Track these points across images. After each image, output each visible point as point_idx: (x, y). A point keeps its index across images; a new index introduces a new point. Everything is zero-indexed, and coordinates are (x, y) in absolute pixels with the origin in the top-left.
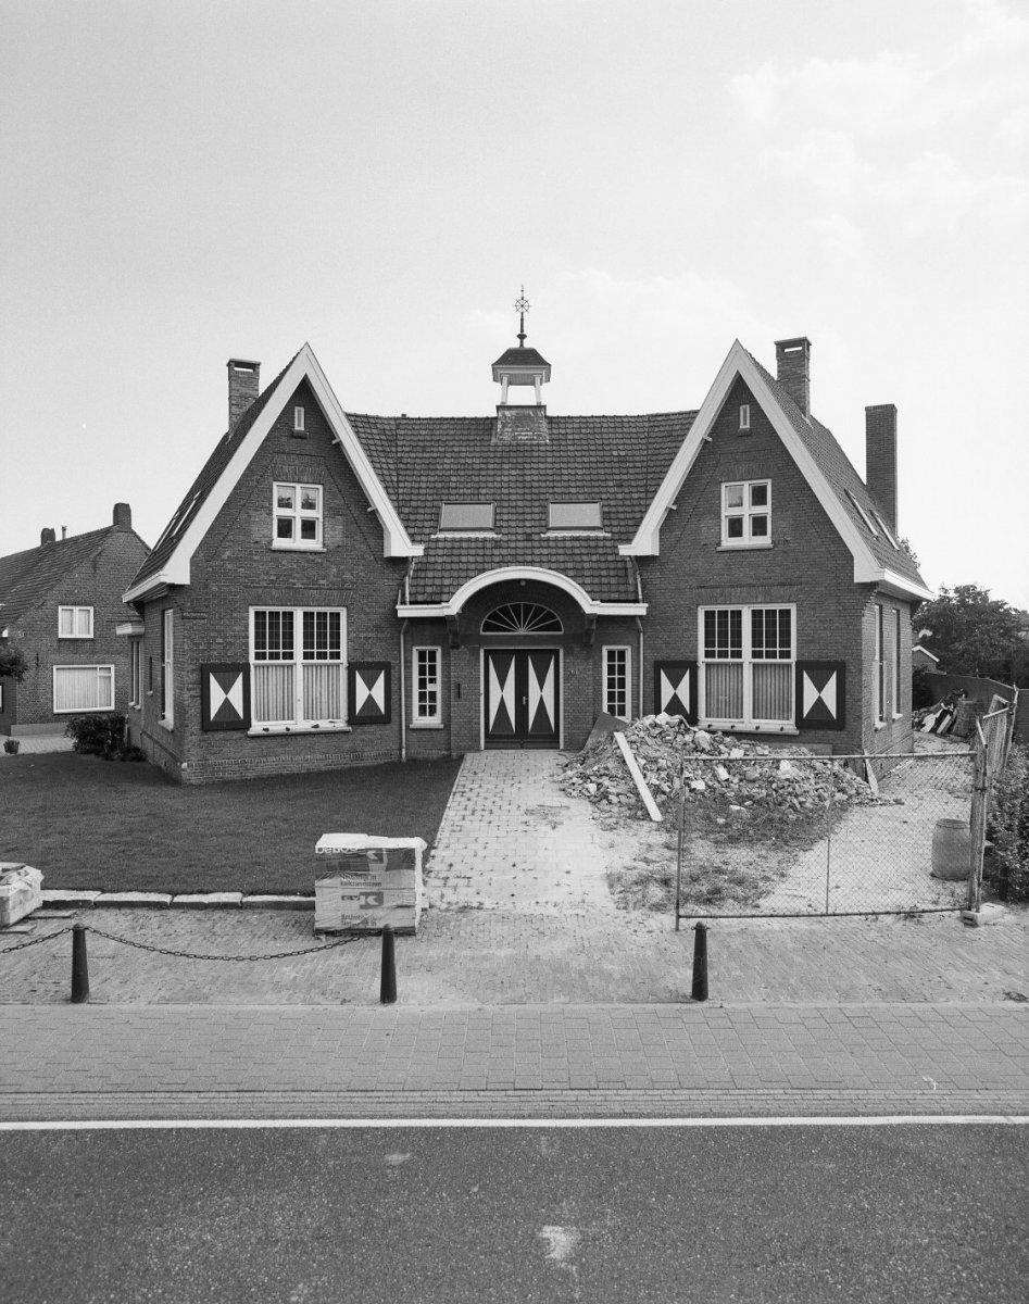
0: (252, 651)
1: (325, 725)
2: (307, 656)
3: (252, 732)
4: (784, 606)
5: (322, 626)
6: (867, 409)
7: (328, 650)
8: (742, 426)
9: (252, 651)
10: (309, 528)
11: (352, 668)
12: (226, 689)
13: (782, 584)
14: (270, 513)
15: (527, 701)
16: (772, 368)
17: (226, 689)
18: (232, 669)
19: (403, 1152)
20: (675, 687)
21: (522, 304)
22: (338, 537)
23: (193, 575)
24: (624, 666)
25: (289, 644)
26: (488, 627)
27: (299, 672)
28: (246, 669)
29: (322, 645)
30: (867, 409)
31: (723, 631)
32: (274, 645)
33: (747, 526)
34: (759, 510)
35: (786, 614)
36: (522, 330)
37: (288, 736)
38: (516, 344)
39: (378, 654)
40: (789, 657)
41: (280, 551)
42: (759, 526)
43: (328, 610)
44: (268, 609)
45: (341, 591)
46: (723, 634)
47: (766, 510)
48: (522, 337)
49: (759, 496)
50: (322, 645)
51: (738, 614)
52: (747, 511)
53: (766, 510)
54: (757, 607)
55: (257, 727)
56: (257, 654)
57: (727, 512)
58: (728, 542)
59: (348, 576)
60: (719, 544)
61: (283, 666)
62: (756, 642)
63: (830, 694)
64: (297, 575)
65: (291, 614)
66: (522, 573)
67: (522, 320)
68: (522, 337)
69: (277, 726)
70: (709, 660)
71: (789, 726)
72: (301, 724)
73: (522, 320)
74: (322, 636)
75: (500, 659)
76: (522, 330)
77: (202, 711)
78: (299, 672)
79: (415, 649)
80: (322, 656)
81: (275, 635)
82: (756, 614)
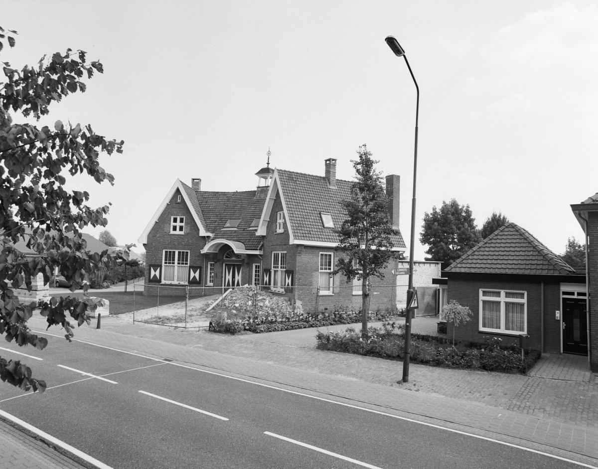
0: (163, 261)
1: (182, 283)
2: (179, 263)
3: (162, 283)
4: (187, 251)
5: (183, 255)
7: (171, 262)
8: (178, 201)
9: (163, 261)
10: (181, 229)
11: (190, 267)
12: (155, 271)
13: (285, 245)
14: (170, 224)
16: (190, 185)
17: (155, 271)
18: (157, 266)
20: (195, 276)
21: (269, 153)
22: (188, 231)
23: (148, 241)
25: (174, 260)
26: (227, 257)
27: (176, 268)
28: (161, 266)
29: (183, 261)
31: (170, 257)
32: (183, 261)
33: (178, 228)
34: (175, 224)
35: (187, 253)
37: (171, 285)
38: (265, 166)
39: (198, 264)
41: (173, 235)
42: (181, 229)
43: (185, 251)
44: (168, 250)
45: (188, 246)
46: (183, 258)
47: (183, 224)
48: (268, 164)
49: (182, 221)
50: (170, 260)
51: (174, 252)
52: (178, 224)
53: (183, 224)
54: (166, 250)
55: (163, 282)
56: (321, 268)
57: (279, 221)
58: (172, 232)
59: (190, 241)
60: (170, 232)
61: (185, 267)
62: (179, 260)
63: (197, 275)
64: (176, 242)
65: (175, 252)
68: (268, 164)
69: (168, 282)
70: (275, 269)
71: (187, 283)
72: (175, 282)
74: (183, 258)
75: (229, 266)
78: (176, 268)
79: (254, 264)
80: (170, 263)
81: (170, 257)
82: (179, 252)
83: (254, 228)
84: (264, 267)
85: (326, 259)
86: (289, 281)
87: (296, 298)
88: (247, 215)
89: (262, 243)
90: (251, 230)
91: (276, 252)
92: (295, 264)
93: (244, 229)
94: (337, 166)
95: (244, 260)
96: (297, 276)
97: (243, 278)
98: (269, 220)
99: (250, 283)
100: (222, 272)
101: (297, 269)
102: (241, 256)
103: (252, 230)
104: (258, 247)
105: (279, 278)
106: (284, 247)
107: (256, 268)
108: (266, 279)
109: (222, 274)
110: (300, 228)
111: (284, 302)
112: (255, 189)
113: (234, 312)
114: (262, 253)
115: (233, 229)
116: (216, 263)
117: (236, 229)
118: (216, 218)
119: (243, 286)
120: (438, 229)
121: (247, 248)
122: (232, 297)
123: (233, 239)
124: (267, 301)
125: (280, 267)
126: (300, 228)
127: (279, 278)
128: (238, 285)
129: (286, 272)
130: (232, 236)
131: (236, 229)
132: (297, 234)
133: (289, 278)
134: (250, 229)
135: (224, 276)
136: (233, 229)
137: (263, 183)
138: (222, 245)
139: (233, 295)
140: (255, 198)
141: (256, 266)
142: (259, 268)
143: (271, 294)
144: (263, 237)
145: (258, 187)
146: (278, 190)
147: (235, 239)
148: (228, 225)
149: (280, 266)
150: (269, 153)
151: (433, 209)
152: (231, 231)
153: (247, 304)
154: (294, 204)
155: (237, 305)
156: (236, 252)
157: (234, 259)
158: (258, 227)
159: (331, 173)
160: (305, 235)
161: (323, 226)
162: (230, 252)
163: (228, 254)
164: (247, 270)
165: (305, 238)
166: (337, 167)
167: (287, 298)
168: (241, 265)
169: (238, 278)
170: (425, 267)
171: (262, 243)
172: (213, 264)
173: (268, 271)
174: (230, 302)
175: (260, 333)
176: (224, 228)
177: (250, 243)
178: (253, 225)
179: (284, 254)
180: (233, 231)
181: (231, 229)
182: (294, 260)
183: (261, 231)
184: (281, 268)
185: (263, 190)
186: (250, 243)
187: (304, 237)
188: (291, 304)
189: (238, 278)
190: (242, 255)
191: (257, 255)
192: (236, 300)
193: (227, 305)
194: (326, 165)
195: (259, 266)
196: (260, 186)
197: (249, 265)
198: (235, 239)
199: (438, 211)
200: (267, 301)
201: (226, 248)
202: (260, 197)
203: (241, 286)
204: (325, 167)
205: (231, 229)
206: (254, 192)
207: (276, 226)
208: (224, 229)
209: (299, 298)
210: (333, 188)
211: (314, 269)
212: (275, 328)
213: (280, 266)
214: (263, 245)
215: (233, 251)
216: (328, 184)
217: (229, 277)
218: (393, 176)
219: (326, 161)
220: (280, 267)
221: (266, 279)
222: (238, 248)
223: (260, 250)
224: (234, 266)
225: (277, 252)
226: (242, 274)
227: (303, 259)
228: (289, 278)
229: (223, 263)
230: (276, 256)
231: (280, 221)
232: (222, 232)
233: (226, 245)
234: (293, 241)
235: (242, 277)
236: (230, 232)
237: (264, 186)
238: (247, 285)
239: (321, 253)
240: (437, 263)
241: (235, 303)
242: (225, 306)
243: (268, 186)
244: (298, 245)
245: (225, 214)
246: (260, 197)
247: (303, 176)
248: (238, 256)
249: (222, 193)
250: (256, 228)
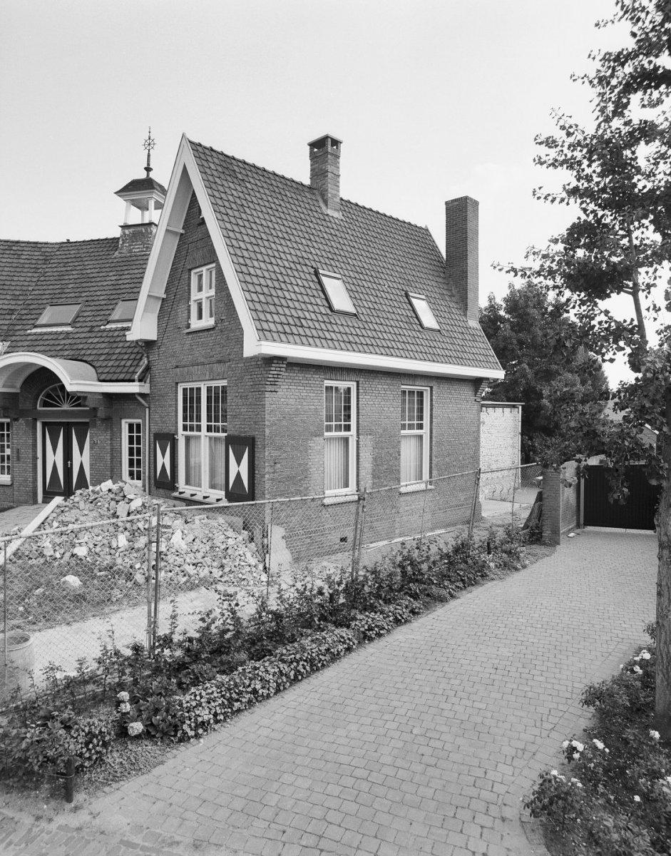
6: (447, 203)
13: (219, 362)
15: (72, 464)
19: (607, 746)
24: (130, 432)
26: (45, 404)
30: (447, 203)
36: (148, 164)
40: (349, 430)
48: (148, 169)
51: (199, 389)
57: (195, 295)
66: (23, 357)
67: (149, 156)
68: (148, 169)
70: (188, 433)
73: (149, 156)
75: (52, 428)
76: (148, 164)
77: (254, 470)
79: (123, 421)
82: (209, 389)
83: (120, 325)
84: (155, 429)
85: (411, 402)
86: (240, 469)
87: (267, 520)
88: (99, 293)
89: (145, 361)
90: (110, 330)
91: (189, 385)
92: (259, 421)
93: (92, 327)
94: (341, 160)
95: (95, 409)
96: (267, 455)
97: (95, 459)
98: (164, 296)
99: (115, 475)
100: (35, 446)
101: (267, 431)
102: (85, 398)
103: (116, 330)
104: (134, 373)
105: (201, 452)
106: (218, 368)
107: (131, 430)
108: (163, 460)
109: (35, 451)
110: (272, 308)
111: (230, 533)
112: (117, 233)
113: (73, 581)
114: (145, 389)
115: (60, 329)
116: (16, 420)
117: (69, 329)
118: (14, 302)
119: (98, 488)
120: (510, 338)
121: (103, 377)
122: (65, 524)
123: (61, 353)
124: (178, 535)
125: (204, 428)
126: (272, 308)
127: (201, 452)
128: (82, 483)
129: (230, 441)
130: (59, 348)
131: (69, 329)
132: (265, 326)
133: (239, 462)
134: (108, 327)
135: (40, 454)
136: (60, 329)
137: (135, 217)
138: (33, 369)
139: (68, 517)
140: (117, 253)
141: (131, 426)
142: (138, 431)
143: (182, 507)
144: (149, 344)
145: (124, 227)
146: (194, 195)
147: (66, 353)
148: (43, 319)
149: (204, 423)
150: (149, 143)
151: (490, 300)
152: (56, 333)
153: (114, 545)
154: (246, 238)
155: (81, 551)
156: (69, 388)
157: (66, 407)
158: (131, 320)
159: (330, 175)
160: (287, 329)
161: (330, 307)
162: (54, 389)
163: (48, 396)
164: (103, 437)
165: (290, 337)
166: (343, 160)
167: (239, 521)
168: (86, 424)
169: (82, 459)
170: (495, 414)
171: (145, 361)
172: (8, 424)
173: (167, 439)
174: (58, 540)
175: (197, 736)
176: (36, 327)
177: (111, 363)
178: (116, 318)
179: (217, 388)
180: (61, 333)
181: (54, 329)
182: (259, 405)
183: (143, 327)
184: (209, 429)
185: (139, 233)
186: (111, 363)
187: (285, 335)
188: (252, 540)
189: (82, 459)
190: (89, 396)
191: (133, 394)
192: (76, 534)
193: (48, 552)
194: (313, 157)
195: (138, 426)
196: (130, 223)
197: (110, 423)
198: (66, 353)
199: (499, 301)
200: (178, 535)
201: (43, 378)
202: (130, 251)
203: (91, 488)
204: (308, 162)
205: (54, 329)
206: (115, 240)
207: (189, 312)
208: (34, 331)
209: (611, 696)
210: (336, 215)
211: (312, 429)
212: (255, 692)
213: (204, 423)
214: (148, 369)
215: (63, 387)
216: (322, 205)
217: (55, 458)
218: (466, 198)
219: (312, 145)
220: (204, 428)
221: (163, 460)
222: (76, 378)
223: (140, 381)
224: (68, 427)
225: (195, 385)
226: (92, 448)
227: (286, 399)
228: (239, 462)
229: (35, 420)
230: (191, 399)
231: (202, 294)
232: (30, 338)
233: (44, 370)
234: (253, 345)
235: (92, 456)
236: (55, 337)
237: (140, 223)
238: (108, 484)
239: (328, 383)
240: (514, 406)
241: (74, 546)
242: (43, 556)
243: (151, 224)
244: (270, 360)
245: (36, 292)
246: (130, 251)
247: (260, 172)
248: (78, 399)
249: (28, 243)
250: (125, 325)
